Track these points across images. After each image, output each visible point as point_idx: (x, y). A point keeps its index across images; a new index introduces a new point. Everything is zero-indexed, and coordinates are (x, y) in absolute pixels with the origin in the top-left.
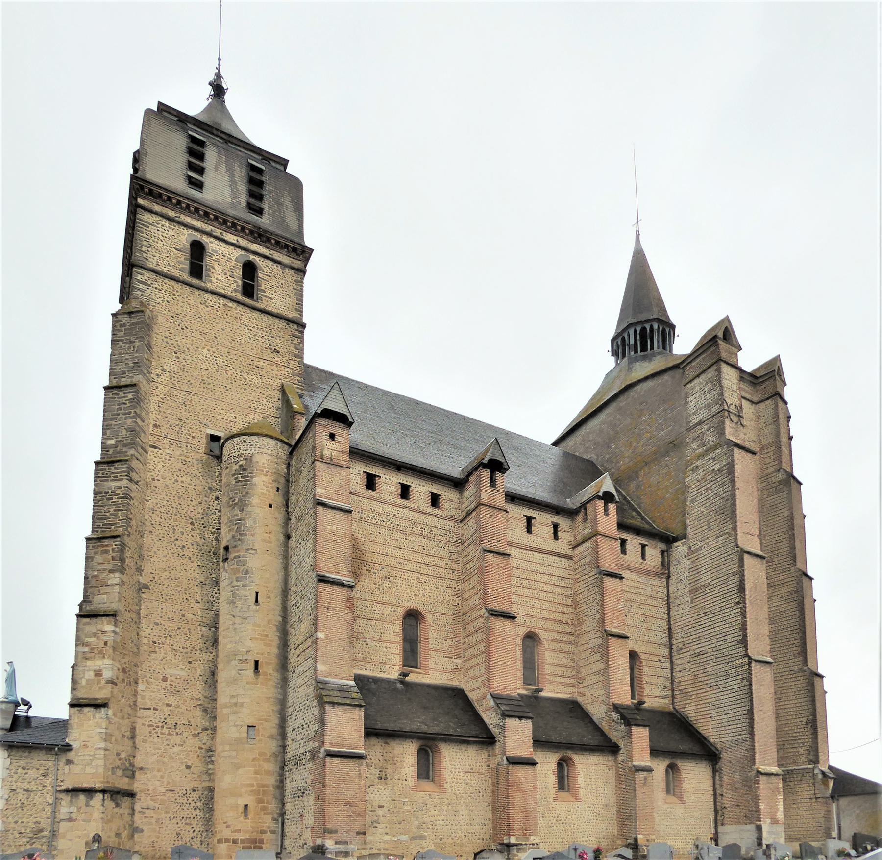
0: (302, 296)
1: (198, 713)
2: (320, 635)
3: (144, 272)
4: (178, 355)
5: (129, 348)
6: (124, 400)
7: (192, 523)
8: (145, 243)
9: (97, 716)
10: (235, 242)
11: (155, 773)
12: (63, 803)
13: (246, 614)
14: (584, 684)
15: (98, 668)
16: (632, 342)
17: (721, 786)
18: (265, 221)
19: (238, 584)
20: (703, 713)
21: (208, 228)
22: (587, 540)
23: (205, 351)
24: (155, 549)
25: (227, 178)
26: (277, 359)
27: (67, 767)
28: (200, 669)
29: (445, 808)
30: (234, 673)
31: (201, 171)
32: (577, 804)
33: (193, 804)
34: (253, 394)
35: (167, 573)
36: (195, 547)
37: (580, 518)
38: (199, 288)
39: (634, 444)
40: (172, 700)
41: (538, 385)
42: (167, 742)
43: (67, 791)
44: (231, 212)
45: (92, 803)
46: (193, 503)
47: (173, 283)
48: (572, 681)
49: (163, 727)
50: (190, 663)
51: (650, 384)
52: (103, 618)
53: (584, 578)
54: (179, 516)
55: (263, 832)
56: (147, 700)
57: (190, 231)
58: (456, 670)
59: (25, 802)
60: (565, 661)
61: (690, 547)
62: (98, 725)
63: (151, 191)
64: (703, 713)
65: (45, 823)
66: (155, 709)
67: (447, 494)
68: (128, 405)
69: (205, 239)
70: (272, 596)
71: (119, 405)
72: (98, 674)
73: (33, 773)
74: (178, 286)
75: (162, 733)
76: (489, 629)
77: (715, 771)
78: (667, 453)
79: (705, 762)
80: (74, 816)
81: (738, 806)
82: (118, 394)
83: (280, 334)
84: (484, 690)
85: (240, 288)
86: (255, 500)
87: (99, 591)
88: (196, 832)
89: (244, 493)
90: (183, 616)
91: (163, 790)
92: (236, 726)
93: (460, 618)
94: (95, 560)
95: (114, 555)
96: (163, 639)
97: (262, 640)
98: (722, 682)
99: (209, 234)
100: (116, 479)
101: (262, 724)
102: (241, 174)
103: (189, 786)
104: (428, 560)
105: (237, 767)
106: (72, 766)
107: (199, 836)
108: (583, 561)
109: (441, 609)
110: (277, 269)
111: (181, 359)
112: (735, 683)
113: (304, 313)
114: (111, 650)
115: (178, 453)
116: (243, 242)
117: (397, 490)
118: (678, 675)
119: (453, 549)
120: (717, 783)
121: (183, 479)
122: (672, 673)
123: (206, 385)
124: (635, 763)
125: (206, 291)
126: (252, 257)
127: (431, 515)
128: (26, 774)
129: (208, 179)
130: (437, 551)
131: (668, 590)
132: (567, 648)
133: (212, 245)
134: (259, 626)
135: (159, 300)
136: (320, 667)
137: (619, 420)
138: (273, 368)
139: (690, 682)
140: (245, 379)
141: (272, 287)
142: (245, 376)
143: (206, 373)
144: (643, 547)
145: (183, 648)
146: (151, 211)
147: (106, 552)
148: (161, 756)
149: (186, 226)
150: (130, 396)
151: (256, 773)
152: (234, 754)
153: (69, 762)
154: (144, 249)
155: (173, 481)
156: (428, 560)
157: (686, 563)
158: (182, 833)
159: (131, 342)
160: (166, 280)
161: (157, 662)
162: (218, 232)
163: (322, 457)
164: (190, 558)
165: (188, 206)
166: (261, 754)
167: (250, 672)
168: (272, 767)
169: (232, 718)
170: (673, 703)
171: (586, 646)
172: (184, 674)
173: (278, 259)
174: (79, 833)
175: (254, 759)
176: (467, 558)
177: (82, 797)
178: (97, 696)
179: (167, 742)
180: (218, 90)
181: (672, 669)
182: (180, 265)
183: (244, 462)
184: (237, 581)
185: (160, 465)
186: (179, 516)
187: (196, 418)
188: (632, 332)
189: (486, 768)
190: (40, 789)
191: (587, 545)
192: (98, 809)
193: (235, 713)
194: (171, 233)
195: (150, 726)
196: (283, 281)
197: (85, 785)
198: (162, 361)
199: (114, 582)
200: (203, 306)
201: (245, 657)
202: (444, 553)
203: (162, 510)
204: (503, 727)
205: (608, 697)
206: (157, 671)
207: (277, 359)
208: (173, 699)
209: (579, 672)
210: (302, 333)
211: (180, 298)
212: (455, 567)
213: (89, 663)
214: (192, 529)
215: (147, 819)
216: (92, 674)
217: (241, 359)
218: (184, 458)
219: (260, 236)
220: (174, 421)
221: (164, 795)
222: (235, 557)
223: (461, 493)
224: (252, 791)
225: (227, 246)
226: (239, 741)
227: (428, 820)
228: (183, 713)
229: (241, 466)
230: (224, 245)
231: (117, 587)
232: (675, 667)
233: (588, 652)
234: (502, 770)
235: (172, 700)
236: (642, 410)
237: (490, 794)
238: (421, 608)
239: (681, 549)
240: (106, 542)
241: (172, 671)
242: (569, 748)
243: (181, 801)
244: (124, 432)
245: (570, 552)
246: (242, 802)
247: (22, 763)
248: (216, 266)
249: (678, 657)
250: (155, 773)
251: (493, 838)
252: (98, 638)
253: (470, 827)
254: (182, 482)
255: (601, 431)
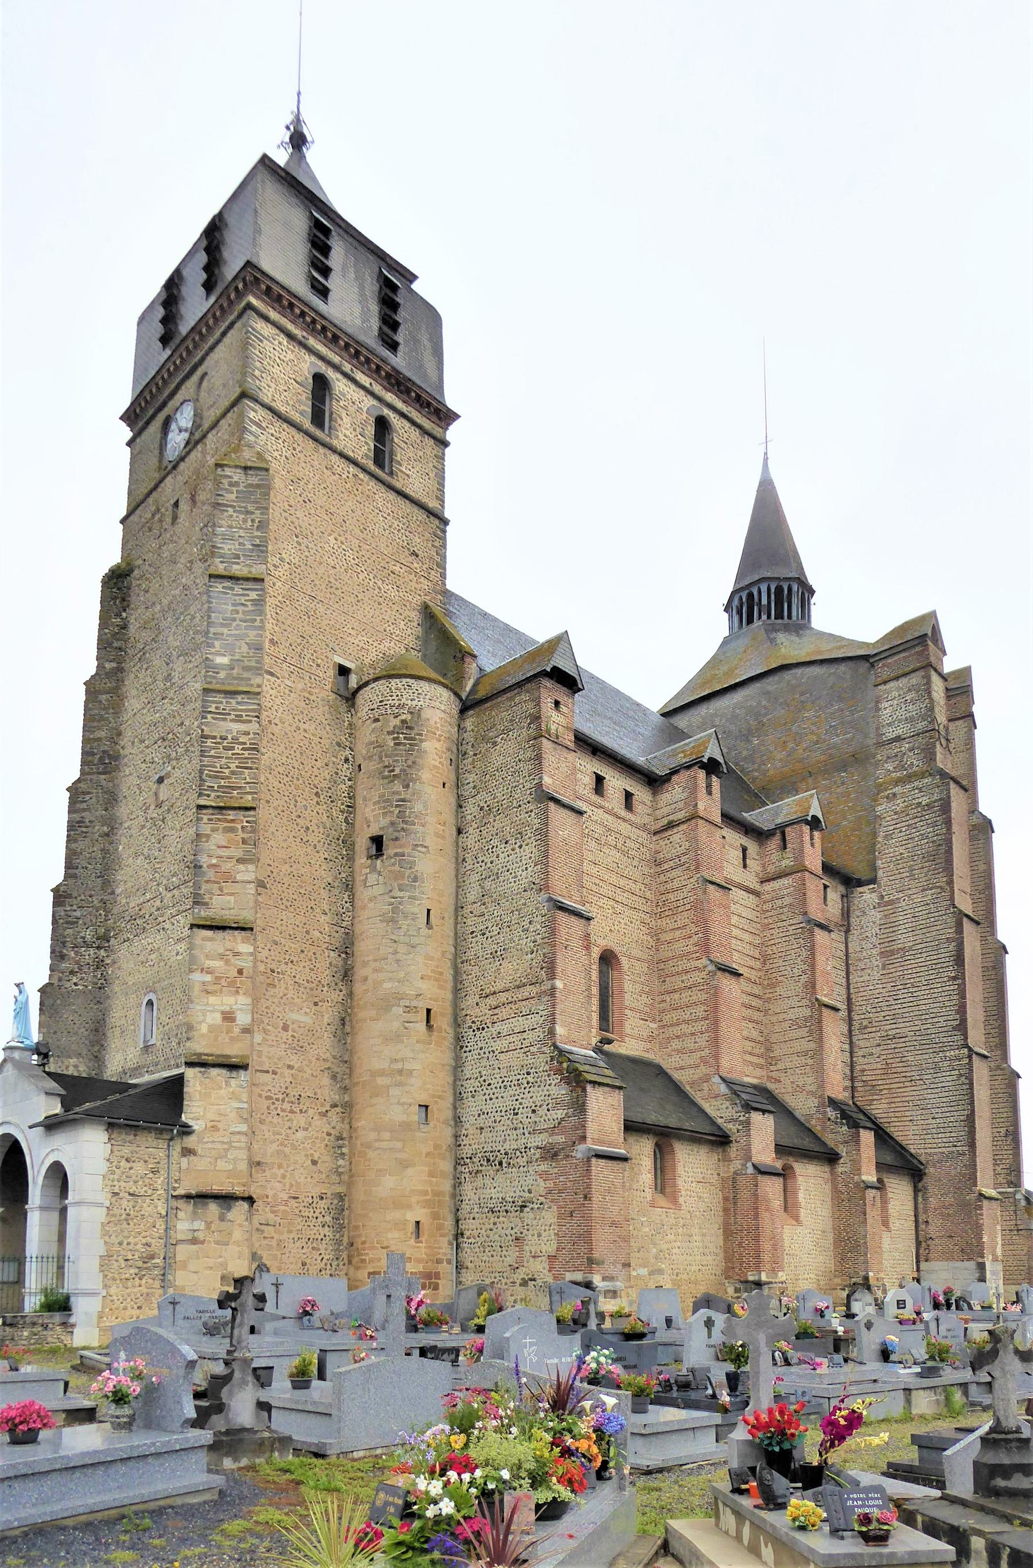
0: (443, 478)
1: (326, 1081)
2: (559, 984)
3: (257, 407)
4: (300, 540)
5: (245, 521)
6: (243, 599)
7: (317, 794)
8: (258, 364)
9: (233, 1082)
10: (368, 385)
11: (275, 1170)
12: (181, 1214)
13: (415, 941)
14: (779, 1067)
15: (228, 1009)
16: (764, 601)
17: (926, 1211)
18: (399, 361)
19: (401, 894)
20: (899, 1114)
21: (337, 359)
22: (786, 875)
23: (331, 538)
24: (273, 829)
25: (356, 290)
26: (415, 565)
27: (184, 1161)
28: (329, 1014)
29: (680, 1231)
30: (396, 1025)
31: (326, 271)
32: (799, 1229)
33: (320, 1219)
34: (389, 612)
35: (287, 866)
36: (322, 830)
37: (775, 842)
38: (324, 445)
39: (791, 745)
40: (294, 1060)
41: (652, 643)
42: (289, 1124)
43: (188, 1197)
44: (362, 338)
45: (230, 1216)
46: (319, 764)
47: (293, 431)
48: (762, 1061)
49: (283, 1100)
50: (316, 1004)
51: (816, 670)
52: (236, 933)
53: (780, 924)
54: (301, 782)
55: (439, 1261)
56: (264, 1059)
57: (313, 358)
58: (651, 1039)
59: (132, 1213)
60: (755, 1034)
61: (882, 897)
62: (234, 1097)
63: (269, 289)
64: (899, 1114)
65: (157, 1246)
66: (274, 1073)
67: (641, 794)
68: (251, 608)
69: (331, 374)
70: (446, 915)
71: (233, 605)
72: (229, 1017)
73: (139, 1168)
74: (299, 437)
75: (283, 1110)
76: (716, 988)
77: (916, 1191)
78: (843, 767)
79: (907, 1178)
80: (200, 1235)
81: (951, 1237)
82: (232, 589)
83: (420, 530)
84: (703, 1070)
85: (372, 454)
86: (425, 775)
87: (221, 889)
88: (324, 1261)
89: (410, 762)
90: (307, 932)
91: (285, 1197)
92: (403, 1104)
93: (659, 967)
94: (212, 841)
95: (245, 836)
96: (283, 967)
97: (436, 980)
98: (930, 1076)
99: (337, 368)
100: (239, 719)
101: (436, 1103)
102: (372, 287)
103: (316, 1191)
104: (623, 882)
105: (404, 1164)
106: (192, 1158)
107: (329, 1267)
108: (779, 903)
109: (636, 953)
110: (414, 434)
111: (303, 547)
112: (948, 1079)
113: (446, 505)
114: (249, 983)
115: (300, 686)
116: (377, 389)
117: (589, 781)
118: (861, 1060)
119: (646, 870)
120: (921, 1206)
121: (306, 726)
122: (852, 1057)
123: (333, 589)
124: (864, 1178)
125: (334, 450)
126: (386, 412)
127: (624, 820)
128: (131, 1168)
129: (333, 283)
130: (629, 871)
131: (847, 947)
132: (756, 1016)
133: (339, 385)
134: (432, 959)
135: (276, 454)
136: (559, 1030)
137: (765, 708)
138: (412, 577)
139: (879, 1072)
140: (379, 588)
141: (409, 459)
142: (380, 583)
143: (333, 571)
144: (826, 887)
145: (308, 981)
146: (266, 319)
147: (232, 830)
148: (282, 1144)
149: (310, 350)
150: (253, 595)
151: (431, 1174)
152: (399, 1145)
153: (187, 1152)
154: (257, 373)
155: (294, 728)
156: (623, 882)
157: (876, 915)
158: (308, 1261)
159: (248, 512)
160: (285, 426)
161: (276, 1000)
162: (347, 367)
163: (548, 731)
164: (315, 847)
165: (303, 314)
166: (436, 1147)
167: (422, 1026)
168: (446, 1166)
169: (394, 1091)
170: (853, 1097)
171: (781, 1017)
172: (308, 1020)
173: (419, 421)
174: (210, 1262)
175: (428, 1154)
176: (669, 886)
177: (213, 1207)
178: (227, 1052)
179: (289, 1124)
180: (298, 140)
181: (851, 1053)
182: (297, 404)
183: (409, 717)
184: (400, 890)
185: (278, 701)
186: (301, 782)
187: (321, 637)
188: (764, 588)
189: (716, 1177)
190: (150, 1192)
191: (785, 881)
192: (240, 1226)
193: (400, 1084)
194: (290, 356)
195: (268, 1098)
196: (421, 453)
197: (216, 1188)
198: (280, 545)
199: (246, 878)
200: (329, 473)
201: (414, 1003)
202: (637, 875)
203: (281, 769)
204: (747, 1123)
205: (821, 1085)
206: (277, 1014)
207: (415, 565)
208: (295, 1057)
209: (769, 1050)
210: (444, 532)
211: (301, 455)
212: (648, 894)
213: (212, 999)
214: (318, 803)
215: (266, 1242)
216: (218, 1017)
217: (374, 557)
218: (307, 695)
219: (398, 384)
220: (295, 638)
221: (286, 1205)
222: (396, 854)
223: (654, 794)
224: (426, 1201)
225: (358, 390)
226: (406, 1126)
227: (665, 1247)
228: (307, 1080)
229: (403, 722)
230: (353, 387)
231: (252, 885)
232: (856, 1050)
233: (787, 1024)
234: (742, 1181)
235: (294, 1060)
236: (802, 702)
237: (721, 1213)
238: (617, 949)
239: (867, 896)
240: (231, 815)
241: (295, 1016)
242: (790, 1154)
243: (306, 1214)
244: (245, 649)
245: (757, 887)
246: (411, 1217)
247: (126, 1151)
248: (344, 415)
249: (861, 1037)
250: (275, 1170)
251: (728, 1272)
252: (227, 962)
253: (703, 1258)
254: (305, 731)
255: (734, 717)
